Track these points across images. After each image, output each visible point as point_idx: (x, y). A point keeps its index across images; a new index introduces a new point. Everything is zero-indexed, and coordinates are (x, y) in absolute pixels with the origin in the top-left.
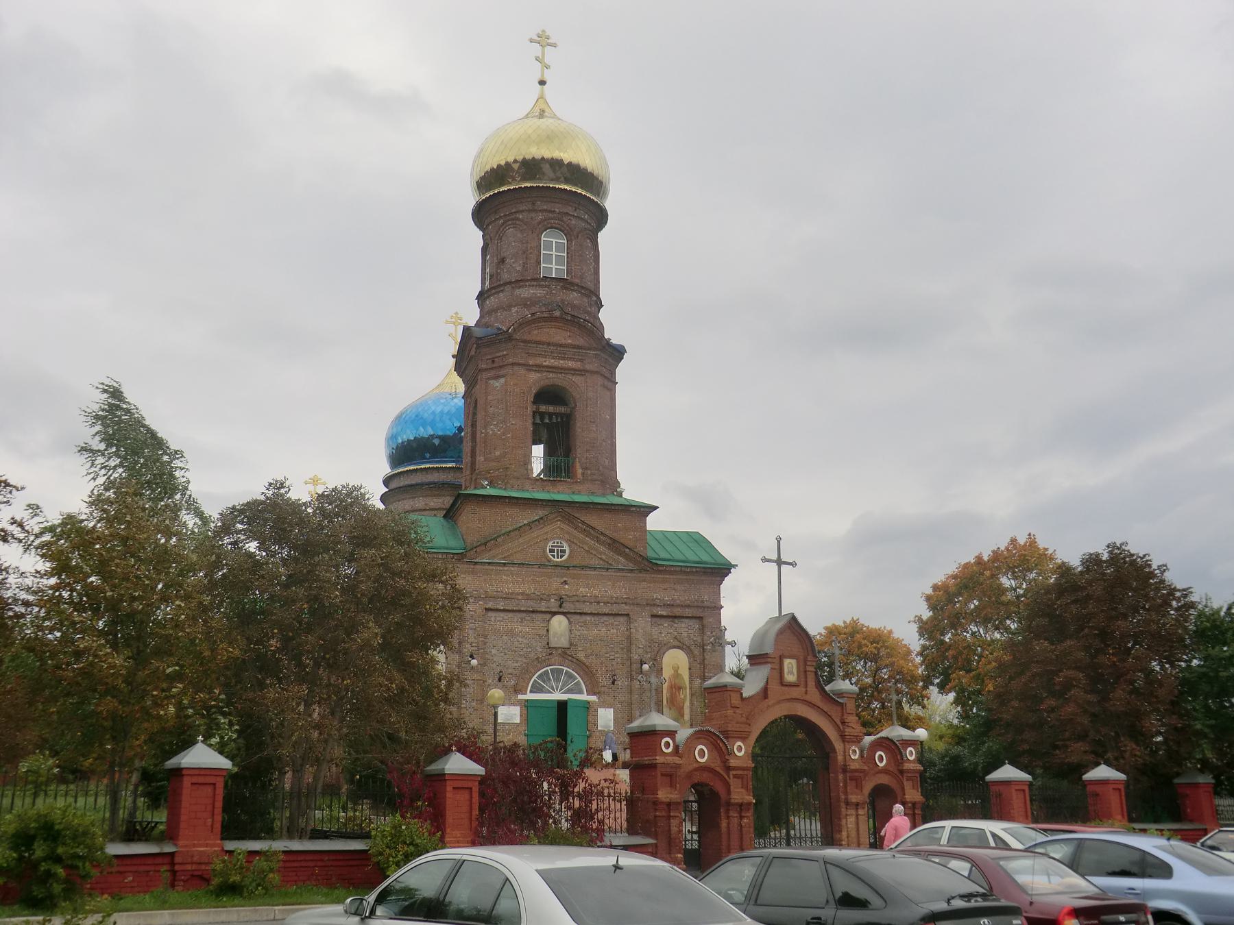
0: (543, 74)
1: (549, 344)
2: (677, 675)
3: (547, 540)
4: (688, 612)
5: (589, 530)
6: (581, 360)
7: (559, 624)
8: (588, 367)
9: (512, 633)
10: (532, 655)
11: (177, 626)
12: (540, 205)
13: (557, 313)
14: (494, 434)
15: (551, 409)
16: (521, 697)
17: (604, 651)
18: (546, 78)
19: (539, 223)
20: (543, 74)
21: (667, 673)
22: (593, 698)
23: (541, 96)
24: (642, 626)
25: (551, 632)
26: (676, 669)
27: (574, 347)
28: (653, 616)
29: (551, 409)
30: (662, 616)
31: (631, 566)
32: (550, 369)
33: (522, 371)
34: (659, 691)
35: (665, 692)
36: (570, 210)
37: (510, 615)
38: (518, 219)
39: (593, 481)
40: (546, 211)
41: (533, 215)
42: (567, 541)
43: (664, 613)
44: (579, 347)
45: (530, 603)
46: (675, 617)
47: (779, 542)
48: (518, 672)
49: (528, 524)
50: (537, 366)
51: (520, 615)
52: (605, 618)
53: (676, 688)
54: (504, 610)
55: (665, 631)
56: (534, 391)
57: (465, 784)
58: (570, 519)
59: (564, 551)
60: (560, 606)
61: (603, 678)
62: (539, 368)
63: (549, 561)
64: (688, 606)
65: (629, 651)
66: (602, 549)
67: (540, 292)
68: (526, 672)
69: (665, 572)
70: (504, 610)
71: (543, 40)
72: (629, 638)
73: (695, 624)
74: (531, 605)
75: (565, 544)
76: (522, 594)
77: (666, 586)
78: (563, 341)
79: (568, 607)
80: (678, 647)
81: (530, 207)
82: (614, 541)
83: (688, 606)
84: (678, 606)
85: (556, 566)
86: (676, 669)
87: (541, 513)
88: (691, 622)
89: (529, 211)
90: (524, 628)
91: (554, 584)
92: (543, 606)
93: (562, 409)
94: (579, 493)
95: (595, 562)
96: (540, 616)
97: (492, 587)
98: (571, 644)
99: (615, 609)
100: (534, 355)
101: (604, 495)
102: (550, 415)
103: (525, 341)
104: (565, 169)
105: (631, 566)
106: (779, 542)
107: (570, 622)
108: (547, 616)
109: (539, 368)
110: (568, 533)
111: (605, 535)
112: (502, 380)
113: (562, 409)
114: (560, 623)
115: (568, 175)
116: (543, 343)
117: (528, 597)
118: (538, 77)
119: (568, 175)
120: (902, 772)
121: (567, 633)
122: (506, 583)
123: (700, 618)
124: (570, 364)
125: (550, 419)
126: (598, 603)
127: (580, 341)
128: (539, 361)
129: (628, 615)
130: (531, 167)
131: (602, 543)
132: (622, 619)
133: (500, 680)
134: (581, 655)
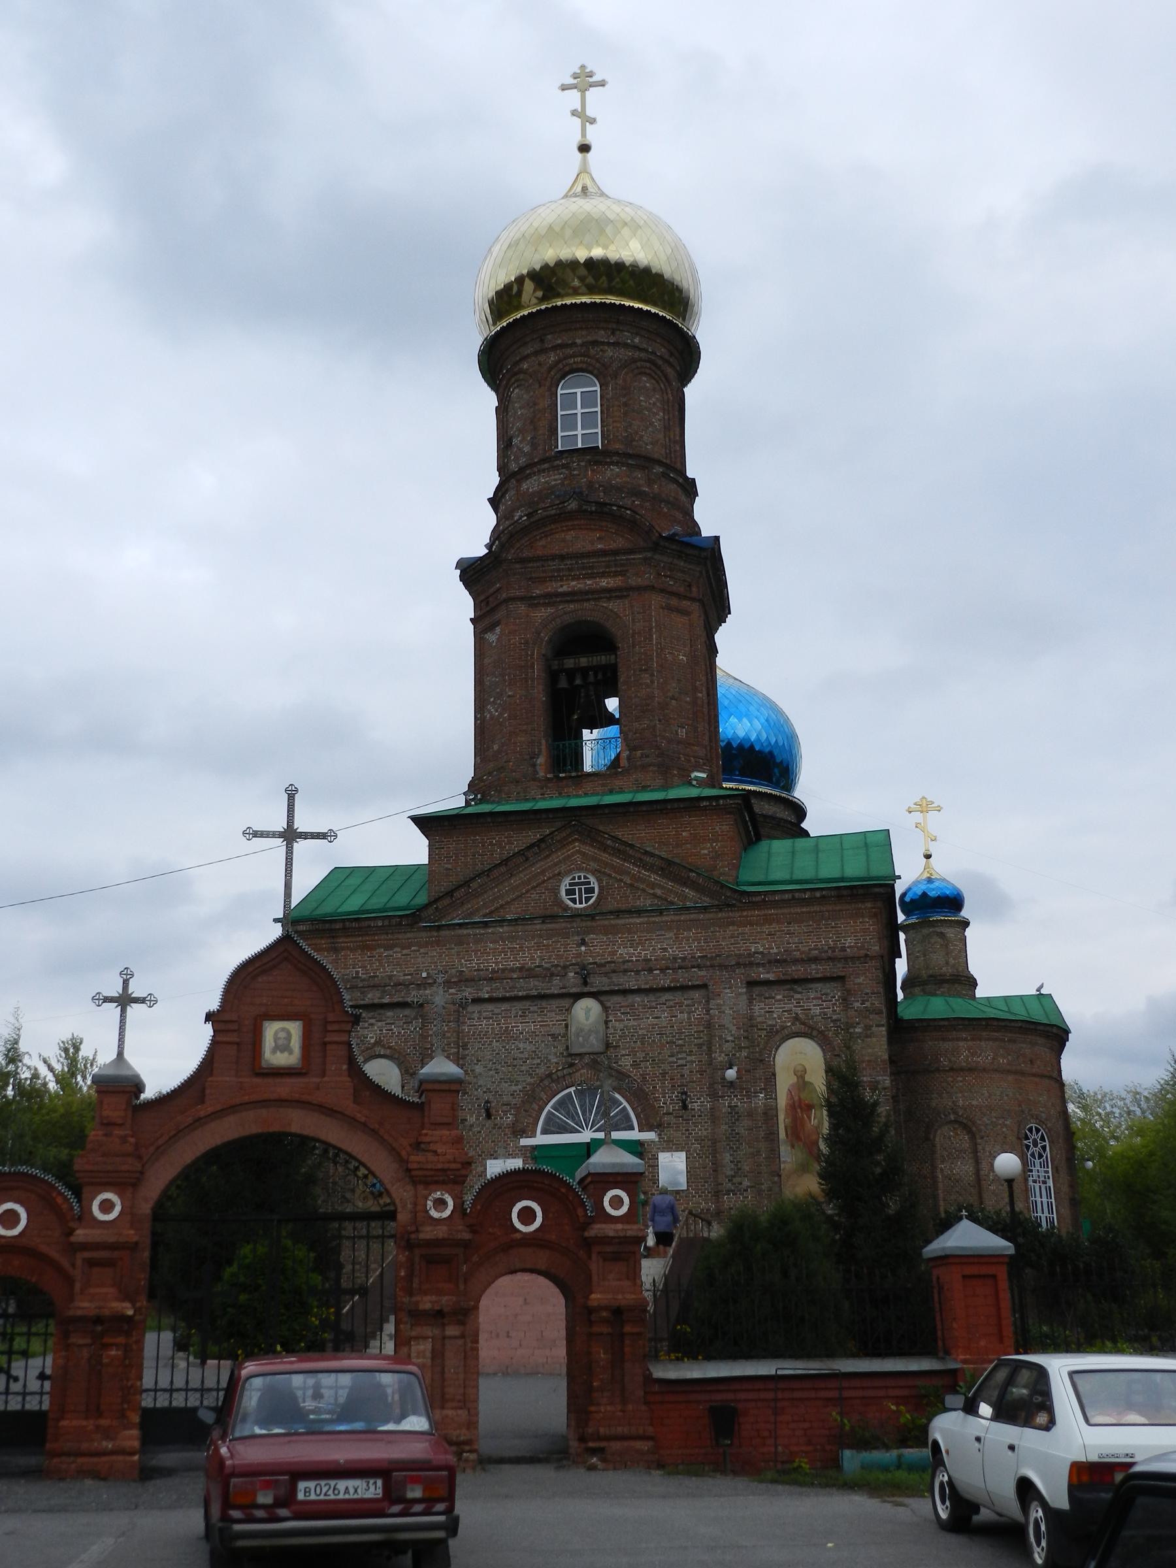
0: (584, 134)
1: (562, 558)
2: (802, 1083)
3: (559, 876)
4: (815, 970)
5: (624, 850)
6: (622, 573)
7: (586, 1012)
8: (633, 581)
9: (506, 1035)
10: (542, 1070)
11: (1031, 1062)
12: (552, 340)
13: (573, 505)
14: (492, 717)
15: (584, 661)
16: (525, 1142)
17: (667, 1052)
18: (591, 139)
19: (551, 369)
20: (584, 134)
21: (784, 1083)
22: (650, 1136)
23: (584, 170)
24: (731, 1001)
25: (573, 1029)
26: (801, 1074)
27: (604, 553)
28: (751, 984)
29: (584, 661)
30: (767, 983)
31: (707, 901)
32: (572, 596)
33: (522, 608)
34: (770, 1114)
35: (781, 1116)
36: (601, 335)
37: (505, 1006)
38: (521, 371)
39: (644, 767)
40: (561, 346)
41: (542, 358)
42: (593, 873)
43: (771, 977)
44: (616, 552)
45: (533, 982)
46: (795, 981)
47: (257, 834)
48: (516, 1101)
49: (520, 853)
50: (548, 595)
51: (519, 1005)
52: (667, 996)
53: (800, 1108)
54: (491, 1000)
55: (777, 1008)
56: (545, 636)
57: (985, 1270)
58: (592, 836)
59: (592, 890)
60: (585, 983)
61: (666, 1101)
62: (551, 599)
63: (567, 908)
64: (815, 960)
65: (710, 1051)
66: (653, 878)
67: (555, 479)
68: (531, 1101)
69: (763, 904)
70: (491, 1000)
71: (584, 81)
72: (709, 1026)
73: (834, 992)
74: (535, 986)
75: (592, 879)
76: (521, 969)
77: (775, 927)
78: (589, 548)
79: (598, 982)
80: (811, 1037)
81: (537, 346)
82: (670, 863)
83: (815, 960)
84: (796, 961)
85: (577, 915)
86: (801, 1074)
87: (532, 836)
88: (827, 988)
89: (536, 353)
90: (527, 1028)
91: (571, 950)
92: (555, 987)
93: (603, 659)
94: (621, 791)
95: (645, 902)
96: (555, 1003)
97: (470, 963)
98: (608, 1045)
99: (683, 977)
100: (542, 580)
101: (665, 787)
102: (584, 671)
103: (523, 561)
104: (583, 272)
105: (707, 901)
106: (257, 834)
107: (605, 1009)
108: (566, 1003)
109: (551, 599)
110: (595, 859)
111: (652, 855)
112: (498, 630)
113: (603, 659)
114: (588, 1011)
115: (590, 280)
116: (553, 557)
117: (528, 973)
118: (577, 139)
119: (590, 280)
120: (588, 1244)
121: (602, 1027)
122: (493, 955)
123: (841, 979)
124: (604, 583)
125: (571, 679)
126: (650, 970)
127: (619, 543)
128: (551, 587)
129: (704, 986)
130: (548, 278)
131: (651, 868)
132: (696, 995)
133: (489, 1116)
134: (626, 1063)
